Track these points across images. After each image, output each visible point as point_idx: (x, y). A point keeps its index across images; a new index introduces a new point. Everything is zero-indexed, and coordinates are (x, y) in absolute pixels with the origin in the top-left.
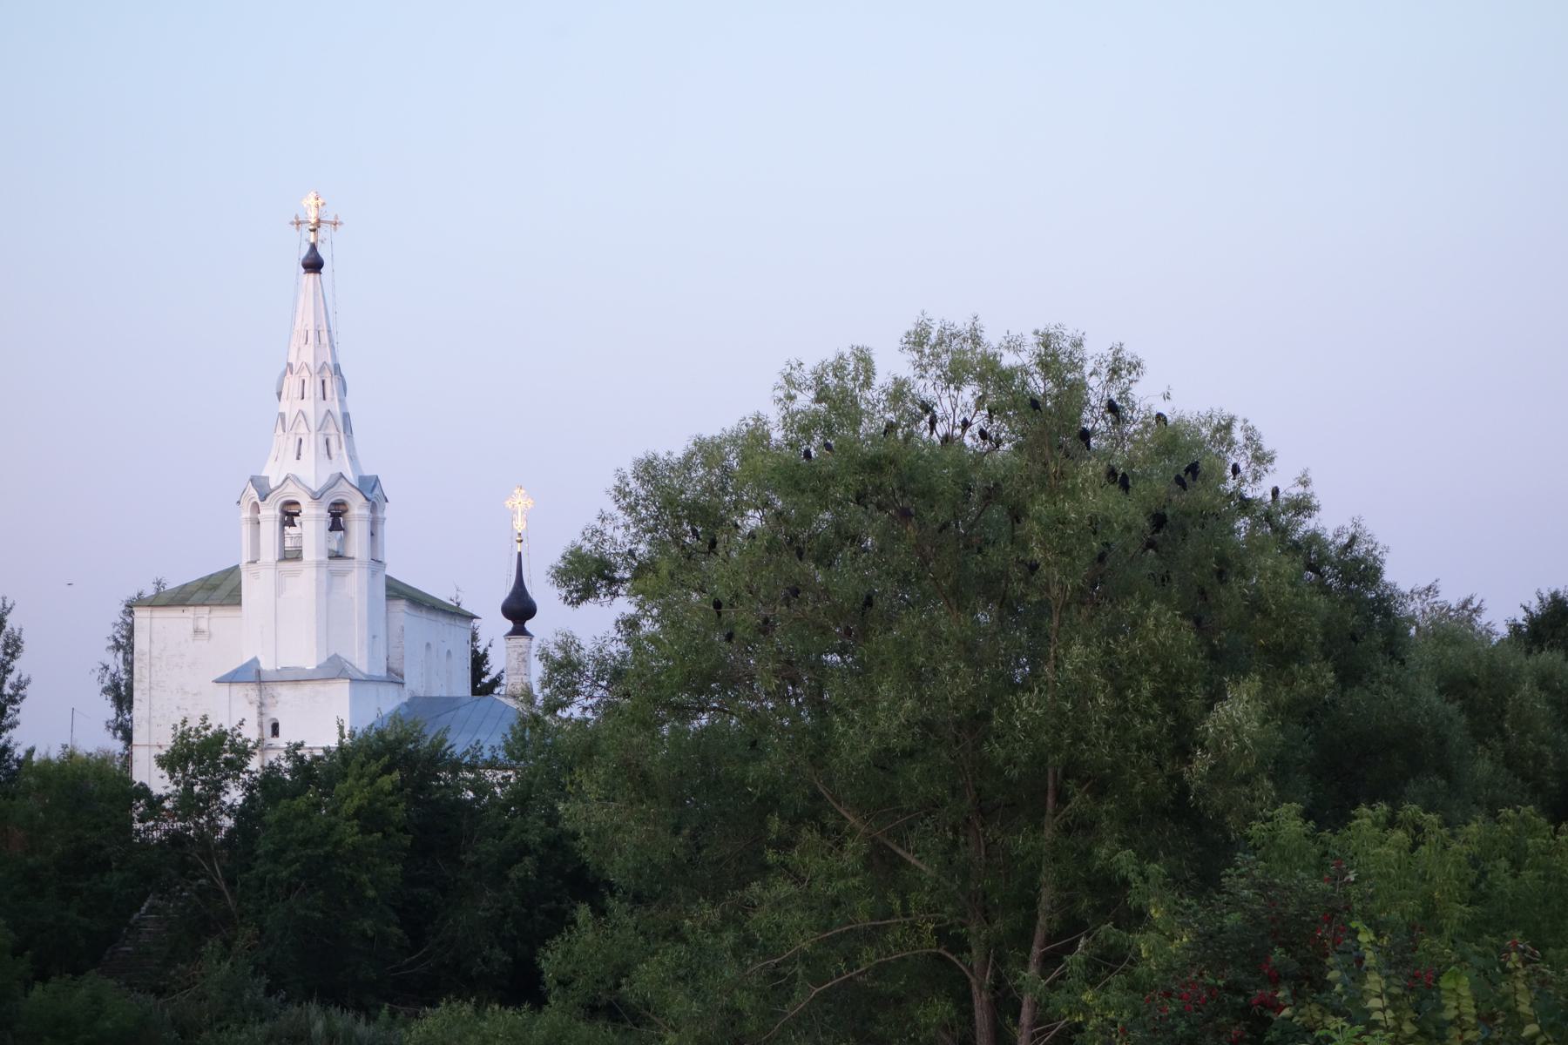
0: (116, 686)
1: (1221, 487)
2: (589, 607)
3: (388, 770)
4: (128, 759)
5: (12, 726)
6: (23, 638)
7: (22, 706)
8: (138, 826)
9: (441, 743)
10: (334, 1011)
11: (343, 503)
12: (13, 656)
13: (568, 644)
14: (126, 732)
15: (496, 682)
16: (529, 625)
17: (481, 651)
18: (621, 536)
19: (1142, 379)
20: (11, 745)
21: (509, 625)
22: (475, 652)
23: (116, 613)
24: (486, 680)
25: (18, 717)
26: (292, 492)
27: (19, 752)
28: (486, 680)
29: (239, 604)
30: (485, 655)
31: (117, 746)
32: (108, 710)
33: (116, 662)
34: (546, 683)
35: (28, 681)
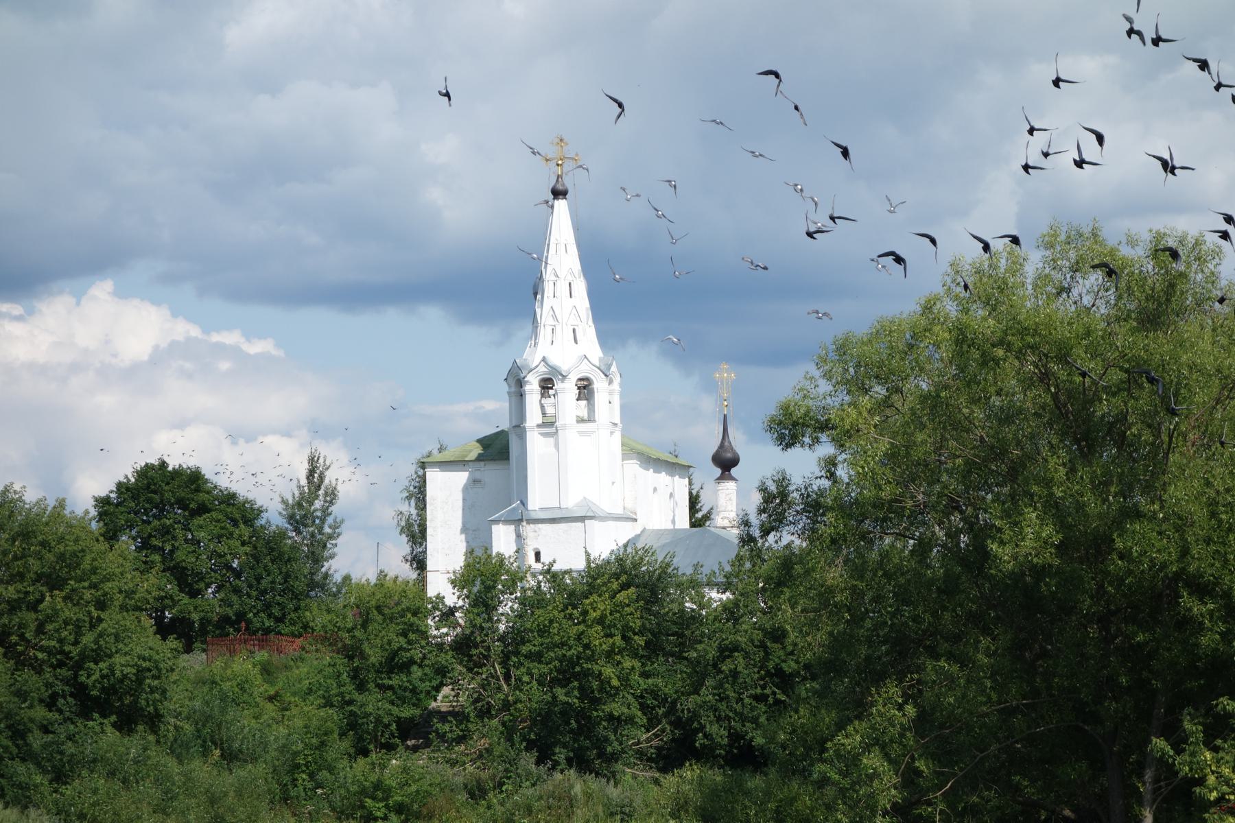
0: (409, 525)
1: (989, 541)
2: (796, 451)
3: (625, 587)
4: (422, 582)
5: (332, 557)
6: (339, 488)
7: (339, 541)
8: (435, 632)
9: (668, 565)
10: (590, 778)
11: (587, 379)
12: (331, 502)
13: (783, 482)
14: (420, 563)
15: (707, 517)
16: (734, 471)
17: (694, 492)
18: (825, 394)
19: (1224, 262)
20: (331, 572)
21: (718, 472)
22: (690, 494)
23: (410, 469)
24: (699, 515)
25: (336, 550)
26: (585, 370)
27: (338, 578)
28: (699, 515)
29: (507, 458)
30: (698, 496)
31: (413, 575)
32: (403, 547)
33: (410, 509)
34: (762, 511)
35: (342, 521)
